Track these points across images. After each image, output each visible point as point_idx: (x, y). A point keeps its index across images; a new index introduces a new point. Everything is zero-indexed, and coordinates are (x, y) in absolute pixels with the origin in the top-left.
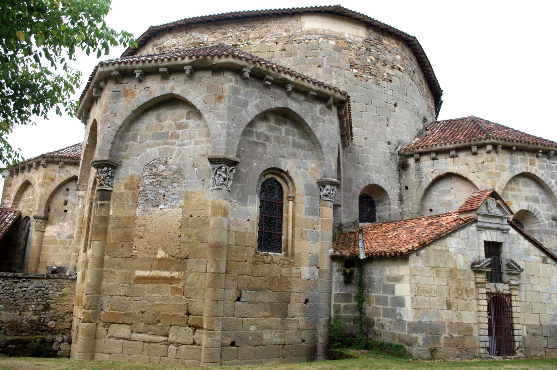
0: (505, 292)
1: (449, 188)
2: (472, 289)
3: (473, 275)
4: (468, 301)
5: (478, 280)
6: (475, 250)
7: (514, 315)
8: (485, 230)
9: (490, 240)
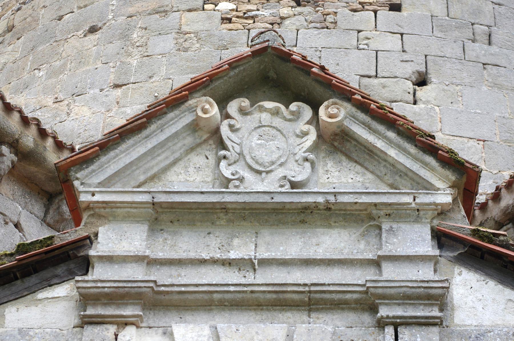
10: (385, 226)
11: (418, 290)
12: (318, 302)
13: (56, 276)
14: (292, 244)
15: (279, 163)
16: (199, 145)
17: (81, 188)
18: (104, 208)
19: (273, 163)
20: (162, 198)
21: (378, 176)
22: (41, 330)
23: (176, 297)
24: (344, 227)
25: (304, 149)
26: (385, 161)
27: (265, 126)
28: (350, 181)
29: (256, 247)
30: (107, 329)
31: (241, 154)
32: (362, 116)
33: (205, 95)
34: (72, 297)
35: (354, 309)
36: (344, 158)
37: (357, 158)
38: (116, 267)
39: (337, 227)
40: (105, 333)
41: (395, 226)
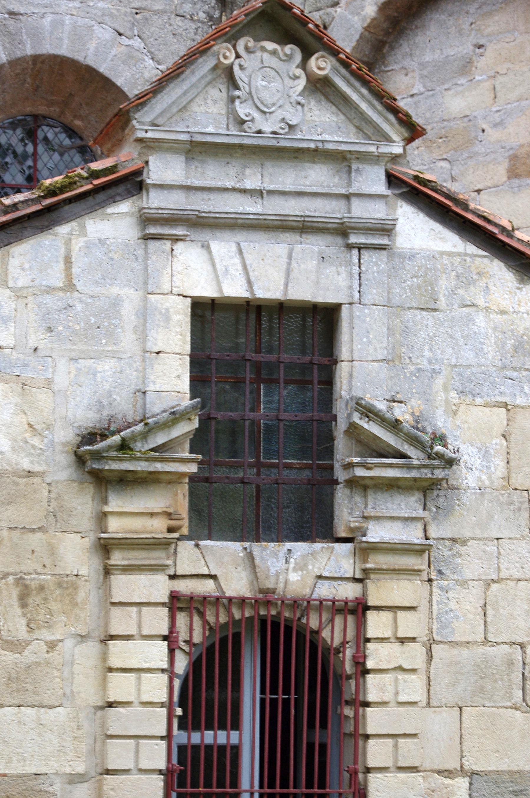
0: (325, 591)
1: (467, 48)
2: (68, 584)
3: (82, 504)
4: (35, 652)
5: (116, 526)
6: (116, 356)
7: (374, 720)
8: (205, 235)
9: (235, 289)
10: (354, 166)
11: (377, 225)
12: (308, 228)
13: (118, 194)
14: (287, 177)
15: (278, 105)
16: (214, 79)
17: (137, 126)
18: (154, 142)
19: (274, 104)
20: (198, 138)
21: (348, 118)
22: (115, 240)
23: (212, 221)
24: (324, 163)
25: (297, 93)
26: (356, 109)
27: (266, 67)
28: (328, 120)
29: (262, 176)
30: (165, 244)
31: (250, 93)
32: (343, 71)
33: (226, 41)
34: (133, 213)
35: (331, 233)
36: (322, 98)
37: (333, 101)
38: (166, 192)
39: (319, 163)
40: (164, 247)
41: (361, 166)
